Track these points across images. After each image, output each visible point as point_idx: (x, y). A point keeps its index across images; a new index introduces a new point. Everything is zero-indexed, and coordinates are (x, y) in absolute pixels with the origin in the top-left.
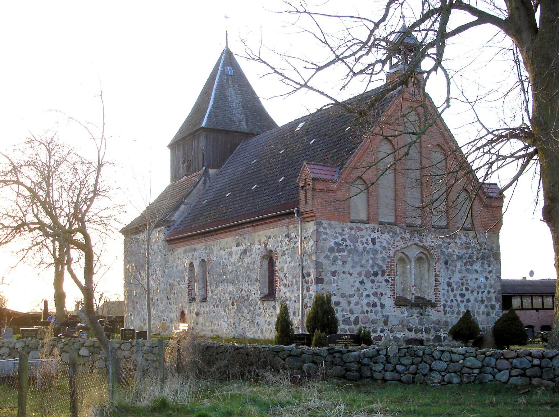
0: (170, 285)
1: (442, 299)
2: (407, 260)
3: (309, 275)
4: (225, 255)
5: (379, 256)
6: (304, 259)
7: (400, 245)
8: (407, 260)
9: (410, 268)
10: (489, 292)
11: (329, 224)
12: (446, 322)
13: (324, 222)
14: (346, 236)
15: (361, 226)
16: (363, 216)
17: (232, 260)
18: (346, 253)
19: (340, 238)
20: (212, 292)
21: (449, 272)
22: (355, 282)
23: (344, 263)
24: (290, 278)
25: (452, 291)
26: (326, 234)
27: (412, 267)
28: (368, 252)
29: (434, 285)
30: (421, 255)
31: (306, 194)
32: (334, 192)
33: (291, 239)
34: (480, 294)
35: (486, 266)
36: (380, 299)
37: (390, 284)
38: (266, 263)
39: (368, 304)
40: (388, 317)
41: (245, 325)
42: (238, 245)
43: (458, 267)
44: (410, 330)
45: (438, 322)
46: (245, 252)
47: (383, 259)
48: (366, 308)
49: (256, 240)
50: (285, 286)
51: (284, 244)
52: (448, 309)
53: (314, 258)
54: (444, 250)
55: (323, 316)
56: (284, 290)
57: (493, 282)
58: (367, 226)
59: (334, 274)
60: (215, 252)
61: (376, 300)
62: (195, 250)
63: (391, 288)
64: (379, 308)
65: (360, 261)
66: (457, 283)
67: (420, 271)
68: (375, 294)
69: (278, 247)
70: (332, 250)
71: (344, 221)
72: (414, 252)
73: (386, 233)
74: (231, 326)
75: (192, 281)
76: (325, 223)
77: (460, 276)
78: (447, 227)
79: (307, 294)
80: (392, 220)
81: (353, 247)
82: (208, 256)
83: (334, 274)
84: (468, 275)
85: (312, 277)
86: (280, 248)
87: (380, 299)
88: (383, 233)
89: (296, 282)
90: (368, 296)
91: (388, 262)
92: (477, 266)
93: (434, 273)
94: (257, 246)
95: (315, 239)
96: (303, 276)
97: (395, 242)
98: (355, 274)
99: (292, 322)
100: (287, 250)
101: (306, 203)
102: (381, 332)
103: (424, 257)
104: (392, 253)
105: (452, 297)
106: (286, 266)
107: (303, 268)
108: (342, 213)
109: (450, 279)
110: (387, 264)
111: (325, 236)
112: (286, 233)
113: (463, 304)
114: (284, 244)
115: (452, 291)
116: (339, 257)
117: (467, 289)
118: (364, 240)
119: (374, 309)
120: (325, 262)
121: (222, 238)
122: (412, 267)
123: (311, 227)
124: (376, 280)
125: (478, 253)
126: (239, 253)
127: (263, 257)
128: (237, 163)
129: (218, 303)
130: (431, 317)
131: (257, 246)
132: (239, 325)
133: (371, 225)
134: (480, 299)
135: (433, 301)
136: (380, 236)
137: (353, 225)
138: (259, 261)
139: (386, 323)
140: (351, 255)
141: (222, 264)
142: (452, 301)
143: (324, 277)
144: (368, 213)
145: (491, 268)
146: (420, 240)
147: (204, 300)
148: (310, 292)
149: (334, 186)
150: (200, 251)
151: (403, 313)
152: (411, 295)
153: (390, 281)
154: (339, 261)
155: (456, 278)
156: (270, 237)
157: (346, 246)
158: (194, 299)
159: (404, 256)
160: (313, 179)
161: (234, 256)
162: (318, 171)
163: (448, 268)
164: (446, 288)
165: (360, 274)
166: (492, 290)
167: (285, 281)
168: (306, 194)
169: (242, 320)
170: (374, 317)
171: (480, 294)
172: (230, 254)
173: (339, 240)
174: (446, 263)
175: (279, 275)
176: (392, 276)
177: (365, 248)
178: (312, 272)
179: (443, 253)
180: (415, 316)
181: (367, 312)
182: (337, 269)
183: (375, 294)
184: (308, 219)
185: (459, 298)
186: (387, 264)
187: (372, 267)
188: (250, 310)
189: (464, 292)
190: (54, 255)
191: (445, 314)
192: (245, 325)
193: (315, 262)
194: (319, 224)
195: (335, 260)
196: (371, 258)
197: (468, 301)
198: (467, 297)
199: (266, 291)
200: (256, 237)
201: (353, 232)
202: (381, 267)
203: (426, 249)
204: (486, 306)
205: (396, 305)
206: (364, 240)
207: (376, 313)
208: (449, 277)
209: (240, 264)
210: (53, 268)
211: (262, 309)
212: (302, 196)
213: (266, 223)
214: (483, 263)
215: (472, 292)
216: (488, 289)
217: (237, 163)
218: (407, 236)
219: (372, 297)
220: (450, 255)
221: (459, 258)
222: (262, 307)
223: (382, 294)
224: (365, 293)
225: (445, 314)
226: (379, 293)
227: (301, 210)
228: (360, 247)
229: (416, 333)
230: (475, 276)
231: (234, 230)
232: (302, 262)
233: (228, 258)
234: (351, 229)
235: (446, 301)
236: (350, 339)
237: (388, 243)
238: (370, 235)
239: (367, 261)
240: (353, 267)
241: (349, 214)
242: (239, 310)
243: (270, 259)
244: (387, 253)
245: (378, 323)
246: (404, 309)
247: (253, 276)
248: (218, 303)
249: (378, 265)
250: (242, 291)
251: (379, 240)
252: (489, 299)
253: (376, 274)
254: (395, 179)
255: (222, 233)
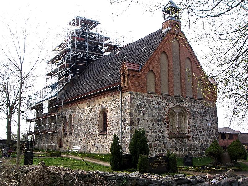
0: (55, 127)
1: (192, 134)
2: (174, 114)
3: (125, 120)
4: (81, 112)
5: (161, 111)
6: (123, 112)
7: (172, 106)
8: (174, 114)
9: (176, 118)
10: (213, 131)
11: (136, 94)
12: (194, 146)
13: (134, 92)
14: (145, 100)
15: (152, 95)
16: (153, 90)
17: (85, 114)
18: (145, 109)
19: (142, 101)
20: (74, 130)
21: (195, 120)
22: (149, 124)
23: (144, 114)
24: (115, 122)
25: (196, 130)
26: (135, 99)
27: (176, 117)
28: (156, 109)
29: (188, 127)
30: (181, 111)
31: (124, 78)
32: (139, 77)
33: (116, 102)
34: (209, 132)
35: (211, 118)
36: (162, 134)
37: (167, 126)
38: (102, 115)
39: (156, 136)
40: (166, 143)
41: (90, 147)
42: (88, 107)
43: (199, 118)
44: (177, 150)
45: (190, 146)
46: (91, 110)
47: (164, 113)
48: (155, 139)
49: (97, 103)
50: (112, 126)
51: (112, 105)
52: (194, 139)
53: (128, 111)
54: (192, 109)
55: (141, 144)
56: (112, 129)
57: (214, 126)
58: (155, 95)
59: (139, 120)
60: (76, 111)
61: (160, 134)
62: (67, 110)
63: (167, 128)
64: (162, 139)
65: (152, 113)
66: (198, 126)
67: (181, 120)
68: (160, 131)
69: (108, 106)
70: (138, 107)
71: (144, 93)
72: (178, 110)
73: (165, 100)
74: (83, 147)
75: (65, 125)
76: (134, 93)
77: (200, 122)
78: (193, 98)
79: (124, 131)
80: (167, 93)
81: (148, 106)
82: (73, 113)
83: (139, 120)
84: (203, 122)
85: (127, 122)
86: (109, 107)
87: (162, 134)
88: (163, 99)
89: (118, 124)
90: (156, 132)
91: (166, 114)
92: (207, 118)
93: (188, 121)
94: (97, 107)
95: (129, 101)
96: (122, 121)
97: (169, 104)
98: (150, 121)
99: (121, 147)
100: (113, 108)
101: (124, 82)
102: (163, 151)
103: (182, 112)
104: (167, 110)
105: (196, 133)
106: (113, 116)
107: (122, 117)
108: (143, 88)
109: (195, 124)
110: (166, 116)
111: (134, 100)
112: (113, 99)
113: (201, 137)
114: (112, 105)
115: (196, 130)
116: (142, 111)
117: (203, 129)
118: (154, 102)
119: (159, 139)
120: (134, 113)
121: (80, 104)
122: (176, 117)
123: (127, 95)
124: (160, 124)
125: (207, 111)
126: (88, 110)
127: (100, 112)
128: (86, 63)
129: (77, 136)
130: (187, 143)
131: (97, 107)
132: (88, 147)
133: (158, 95)
134: (209, 134)
135: (187, 135)
136: (161, 101)
137: (148, 94)
138: (98, 114)
139: (165, 147)
140: (147, 110)
141: (80, 117)
142: (196, 135)
143: (134, 122)
144: (156, 89)
145: (213, 119)
146: (181, 104)
147: (71, 134)
148: (126, 130)
149: (139, 74)
150: (69, 111)
151: (173, 141)
152: (176, 132)
153: (167, 124)
154: (141, 113)
155: (198, 124)
156: (104, 102)
157: (145, 105)
158: (66, 134)
159: (173, 112)
160: (129, 70)
161: (85, 112)
162: (131, 66)
163: (194, 118)
164: (193, 129)
165: (152, 120)
166: (214, 130)
167: (112, 124)
168: (124, 78)
169: (89, 144)
170: (159, 143)
171: (209, 132)
172: (84, 111)
173: (142, 102)
174: (193, 116)
175: (109, 121)
176: (168, 122)
177: (154, 107)
178: (128, 119)
179: (191, 110)
180: (179, 143)
181: (156, 141)
182: (140, 117)
183: (160, 131)
184: (125, 91)
185: (199, 134)
186: (166, 116)
187: (158, 117)
188: (93, 139)
189: (202, 130)
190: (7, 114)
191: (193, 142)
192: (91, 147)
193: (129, 113)
194: (131, 93)
195: (140, 112)
196: (158, 112)
197: (204, 135)
198: (203, 133)
199: (102, 130)
200: (97, 102)
201: (148, 98)
202: (162, 117)
203: (184, 108)
204: (212, 138)
205: (170, 137)
206: (154, 102)
207: (160, 141)
208: (195, 123)
209: (88, 116)
210: (6, 120)
211: (99, 139)
212: (122, 79)
213: (102, 95)
214: (209, 116)
215: (205, 131)
216: (212, 129)
217: (86, 63)
218: (175, 101)
219: (158, 133)
220: (195, 112)
221: (199, 113)
222: (99, 137)
223: (163, 131)
224: (155, 131)
225: (193, 142)
226: (161, 131)
227: (122, 86)
228: (152, 106)
229: (180, 152)
230: (206, 123)
231: (86, 100)
232: (122, 114)
233: (83, 113)
234: (147, 96)
235: (194, 135)
236: (162, 159)
237: (166, 105)
238: (157, 100)
239: (156, 113)
240: (148, 117)
241: (147, 89)
242: (88, 139)
243: (104, 113)
244: (165, 110)
245: (161, 146)
246: (174, 139)
247: (95, 122)
248: (77, 136)
249: (161, 116)
250: (89, 130)
251: (161, 103)
252: (213, 134)
253: (160, 121)
254: (168, 73)
255: (80, 101)
